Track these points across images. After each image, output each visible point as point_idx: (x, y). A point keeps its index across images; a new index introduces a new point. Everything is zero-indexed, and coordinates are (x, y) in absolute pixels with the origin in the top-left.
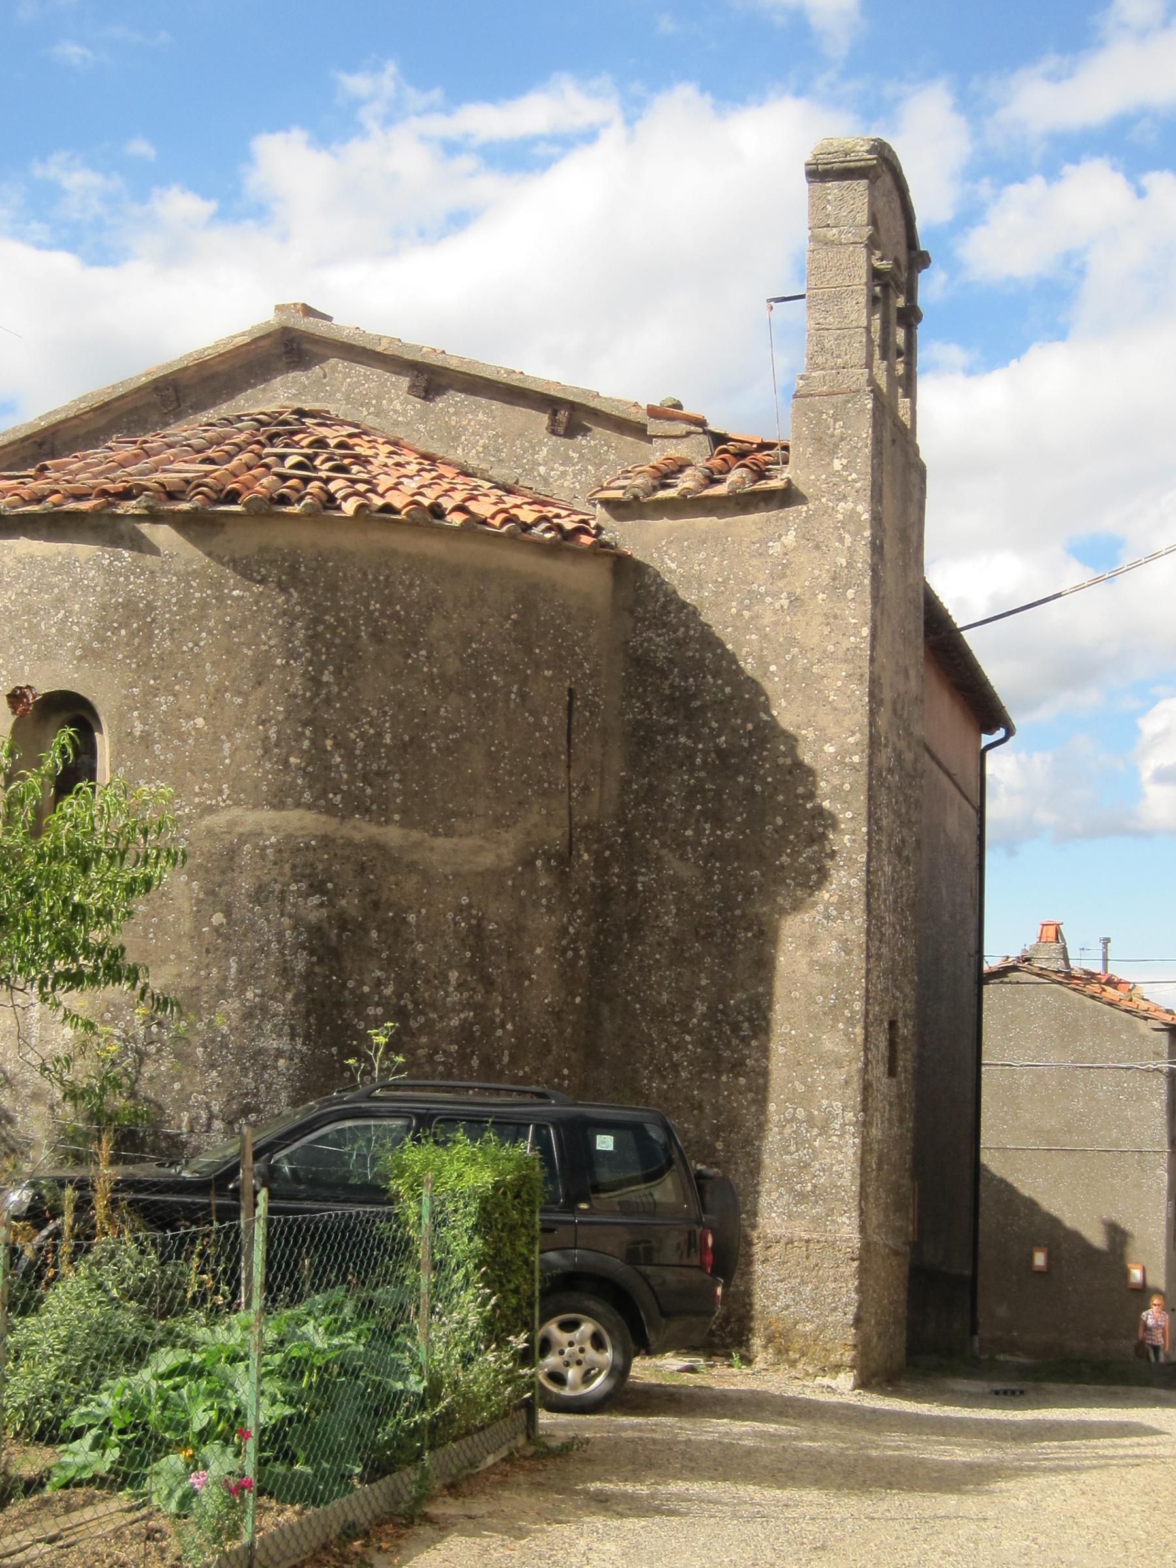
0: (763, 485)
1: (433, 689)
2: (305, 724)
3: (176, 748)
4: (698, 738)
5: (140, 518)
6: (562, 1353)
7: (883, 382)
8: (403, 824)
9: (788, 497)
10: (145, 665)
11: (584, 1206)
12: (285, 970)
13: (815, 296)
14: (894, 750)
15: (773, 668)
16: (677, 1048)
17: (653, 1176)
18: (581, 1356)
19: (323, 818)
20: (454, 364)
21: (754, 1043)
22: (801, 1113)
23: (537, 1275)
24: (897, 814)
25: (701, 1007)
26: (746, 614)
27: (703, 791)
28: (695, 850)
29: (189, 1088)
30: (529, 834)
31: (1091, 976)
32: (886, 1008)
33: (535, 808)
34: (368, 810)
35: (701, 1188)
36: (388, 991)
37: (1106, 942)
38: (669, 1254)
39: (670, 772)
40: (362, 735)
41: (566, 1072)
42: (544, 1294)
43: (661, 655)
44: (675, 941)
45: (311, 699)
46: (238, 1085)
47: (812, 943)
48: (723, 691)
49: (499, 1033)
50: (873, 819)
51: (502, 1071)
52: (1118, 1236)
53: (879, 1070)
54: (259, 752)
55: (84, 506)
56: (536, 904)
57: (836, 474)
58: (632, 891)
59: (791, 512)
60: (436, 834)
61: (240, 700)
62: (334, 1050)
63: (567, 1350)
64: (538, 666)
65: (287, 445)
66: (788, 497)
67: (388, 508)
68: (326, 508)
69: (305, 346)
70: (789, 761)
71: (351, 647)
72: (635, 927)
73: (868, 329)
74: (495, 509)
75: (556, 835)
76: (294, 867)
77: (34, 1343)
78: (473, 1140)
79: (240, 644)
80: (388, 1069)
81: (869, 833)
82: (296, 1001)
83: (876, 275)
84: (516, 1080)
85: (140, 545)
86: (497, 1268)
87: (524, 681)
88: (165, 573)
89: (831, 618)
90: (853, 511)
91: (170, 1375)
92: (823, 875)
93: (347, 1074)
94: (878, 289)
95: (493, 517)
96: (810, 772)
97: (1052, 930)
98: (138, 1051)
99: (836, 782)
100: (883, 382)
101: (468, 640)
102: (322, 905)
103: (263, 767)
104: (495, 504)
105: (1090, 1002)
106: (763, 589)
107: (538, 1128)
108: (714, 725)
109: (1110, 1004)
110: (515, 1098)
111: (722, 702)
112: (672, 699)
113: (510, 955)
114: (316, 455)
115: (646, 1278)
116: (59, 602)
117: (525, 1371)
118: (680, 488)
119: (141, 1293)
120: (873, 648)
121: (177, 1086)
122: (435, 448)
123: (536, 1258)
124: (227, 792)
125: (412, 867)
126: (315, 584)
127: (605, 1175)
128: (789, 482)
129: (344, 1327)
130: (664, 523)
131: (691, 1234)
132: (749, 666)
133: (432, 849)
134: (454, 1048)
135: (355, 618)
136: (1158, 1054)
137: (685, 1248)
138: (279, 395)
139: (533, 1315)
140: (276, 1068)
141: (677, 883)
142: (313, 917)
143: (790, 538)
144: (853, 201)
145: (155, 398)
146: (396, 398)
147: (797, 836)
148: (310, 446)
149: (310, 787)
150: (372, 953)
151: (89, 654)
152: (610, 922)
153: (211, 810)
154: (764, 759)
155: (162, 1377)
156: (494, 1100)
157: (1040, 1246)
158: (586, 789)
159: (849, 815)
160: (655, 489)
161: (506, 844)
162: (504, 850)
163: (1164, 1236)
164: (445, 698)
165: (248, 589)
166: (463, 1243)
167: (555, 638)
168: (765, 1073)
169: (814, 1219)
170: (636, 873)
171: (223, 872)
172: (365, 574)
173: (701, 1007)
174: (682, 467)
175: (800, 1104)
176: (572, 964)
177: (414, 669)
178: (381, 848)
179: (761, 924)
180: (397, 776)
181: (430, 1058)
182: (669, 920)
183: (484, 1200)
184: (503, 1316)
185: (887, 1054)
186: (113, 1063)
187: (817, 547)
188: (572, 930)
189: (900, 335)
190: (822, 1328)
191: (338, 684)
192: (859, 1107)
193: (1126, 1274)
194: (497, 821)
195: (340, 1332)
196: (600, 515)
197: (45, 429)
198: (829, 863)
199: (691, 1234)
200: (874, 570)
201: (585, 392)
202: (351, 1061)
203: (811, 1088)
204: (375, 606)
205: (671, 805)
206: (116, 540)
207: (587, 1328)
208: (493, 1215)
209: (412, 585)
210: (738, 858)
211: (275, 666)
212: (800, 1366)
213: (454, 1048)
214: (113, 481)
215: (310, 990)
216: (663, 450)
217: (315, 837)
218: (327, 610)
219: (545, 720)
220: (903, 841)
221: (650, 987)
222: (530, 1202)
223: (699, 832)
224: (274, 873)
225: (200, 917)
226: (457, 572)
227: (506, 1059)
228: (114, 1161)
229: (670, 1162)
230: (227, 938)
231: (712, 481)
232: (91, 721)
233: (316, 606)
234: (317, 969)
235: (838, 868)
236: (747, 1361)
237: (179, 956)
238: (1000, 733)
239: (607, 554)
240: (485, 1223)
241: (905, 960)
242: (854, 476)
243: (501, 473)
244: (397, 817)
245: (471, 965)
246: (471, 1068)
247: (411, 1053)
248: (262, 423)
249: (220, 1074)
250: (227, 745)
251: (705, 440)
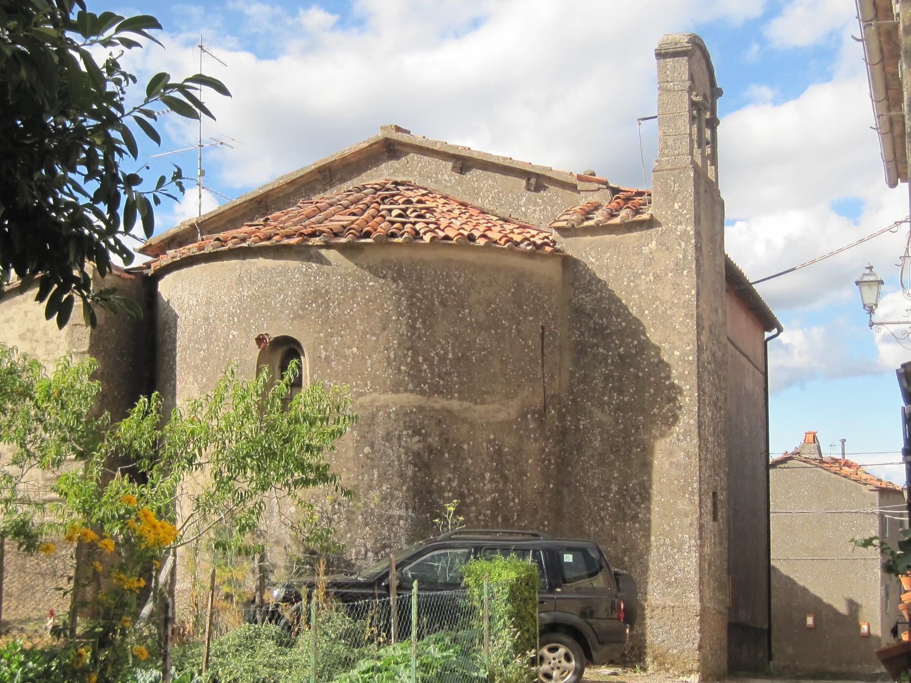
0: (638, 218)
1: (473, 329)
2: (408, 349)
3: (343, 364)
4: (609, 350)
5: (321, 247)
6: (550, 663)
7: (699, 161)
8: (459, 399)
9: (651, 223)
10: (326, 322)
11: (559, 590)
12: (402, 475)
13: (664, 118)
14: (711, 352)
15: (647, 312)
16: (603, 509)
17: (592, 575)
18: (559, 665)
19: (419, 397)
20: (475, 156)
21: (642, 506)
22: (668, 541)
23: (538, 623)
24: (714, 385)
25: (615, 488)
26: (632, 284)
27: (612, 376)
28: (609, 407)
29: (355, 536)
30: (523, 401)
31: (836, 461)
33: (527, 388)
34: (441, 392)
35: (617, 581)
36: (455, 484)
38: (602, 612)
39: (595, 367)
40: (437, 354)
41: (546, 523)
42: (542, 633)
43: (589, 307)
44: (600, 454)
45: (411, 337)
46: (380, 534)
47: (671, 453)
50: (700, 388)
51: (513, 524)
52: (854, 606)
53: (708, 518)
54: (386, 364)
55: (293, 241)
56: (529, 437)
57: (676, 211)
58: (577, 429)
59: (653, 231)
60: (476, 403)
62: (428, 515)
63: (553, 662)
64: (526, 314)
65: (391, 204)
66: (651, 223)
67: (447, 238)
68: (415, 239)
69: (397, 147)
70: (656, 360)
71: (430, 309)
72: (579, 447)
73: (690, 135)
74: (500, 235)
75: (538, 401)
76: (405, 422)
77: (297, 660)
78: (506, 558)
79: (374, 309)
80: (456, 524)
81: (699, 396)
82: (408, 490)
83: (693, 104)
84: (520, 528)
85: (321, 260)
86: (519, 618)
87: (518, 323)
88: (334, 275)
89: (676, 286)
90: (685, 230)
91: (368, 671)
92: (676, 418)
93: (435, 527)
94: (695, 112)
95: (500, 239)
96: (667, 365)
97: (811, 437)
98: (328, 518)
99: (681, 370)
100: (699, 161)
101: (489, 303)
102: (420, 441)
104: (500, 232)
105: (834, 476)
107: (535, 552)
108: (617, 342)
109: (845, 477)
110: (520, 537)
112: (595, 329)
113: (516, 464)
114: (407, 208)
115: (591, 625)
116: (281, 290)
117: (533, 668)
118: (595, 220)
119: (347, 635)
120: (698, 301)
121: (349, 535)
122: (466, 199)
123: (537, 615)
124: (369, 385)
125: (465, 421)
126: (410, 277)
127: (568, 574)
128: (652, 215)
129: (447, 648)
130: (588, 238)
131: (613, 603)
132: (634, 311)
133: (474, 411)
134: (489, 512)
135: (432, 295)
136: (873, 504)
137: (609, 610)
138: (384, 173)
139: (536, 643)
141: (600, 424)
142: (415, 448)
143: (653, 245)
144: (681, 68)
145: (319, 176)
146: (446, 171)
147: (662, 399)
148: (404, 203)
149: (412, 382)
150: (446, 465)
151: (297, 317)
152: (565, 443)
153: (361, 394)
154: (643, 360)
155: (363, 673)
156: (510, 538)
157: (810, 613)
158: (552, 377)
159: (688, 387)
160: (583, 221)
161: (512, 407)
162: (511, 410)
163: (879, 606)
164: (479, 334)
165: (377, 282)
166: (502, 608)
167: (534, 300)
168: (649, 521)
169: (676, 595)
170: (579, 420)
171: (369, 426)
172: (436, 272)
173: (615, 488)
174: (597, 207)
175: (667, 537)
176: (548, 467)
177: (463, 319)
178: (449, 411)
179: (644, 445)
181: (477, 518)
182: (597, 444)
183: (512, 586)
184: (522, 643)
186: (316, 524)
187: (667, 249)
188: (547, 450)
189: (708, 133)
190: (682, 652)
192: (697, 537)
193: (859, 628)
194: (507, 396)
195: (445, 650)
196: (555, 235)
197: (262, 195)
198: (678, 412)
199: (613, 603)
200: (697, 261)
201: (544, 168)
202: (437, 520)
203: (672, 528)
204: (442, 287)
205: (596, 384)
206: (309, 259)
207: (562, 650)
208: (518, 594)
209: (460, 276)
210: (631, 411)
211: (391, 320)
212: (671, 671)
213: (489, 512)
214: (305, 227)
215: (415, 484)
216: (586, 198)
217: (415, 407)
218: (417, 291)
219: (530, 343)
220: (717, 398)
221: (588, 478)
222: (533, 588)
223: (611, 397)
224: (395, 426)
225: (358, 450)
226: (483, 269)
227: (515, 517)
228: (326, 574)
229: (601, 567)
230: (372, 459)
231: (612, 216)
232: (299, 350)
233: (412, 289)
234: (418, 474)
235: (683, 414)
236: (644, 669)
237: (348, 469)
238: (775, 331)
239: (559, 256)
240: (513, 597)
241: (721, 460)
243: (501, 212)
245: (496, 470)
246: (497, 522)
247: (467, 515)
248: (377, 190)
249: (371, 529)
251: (608, 192)
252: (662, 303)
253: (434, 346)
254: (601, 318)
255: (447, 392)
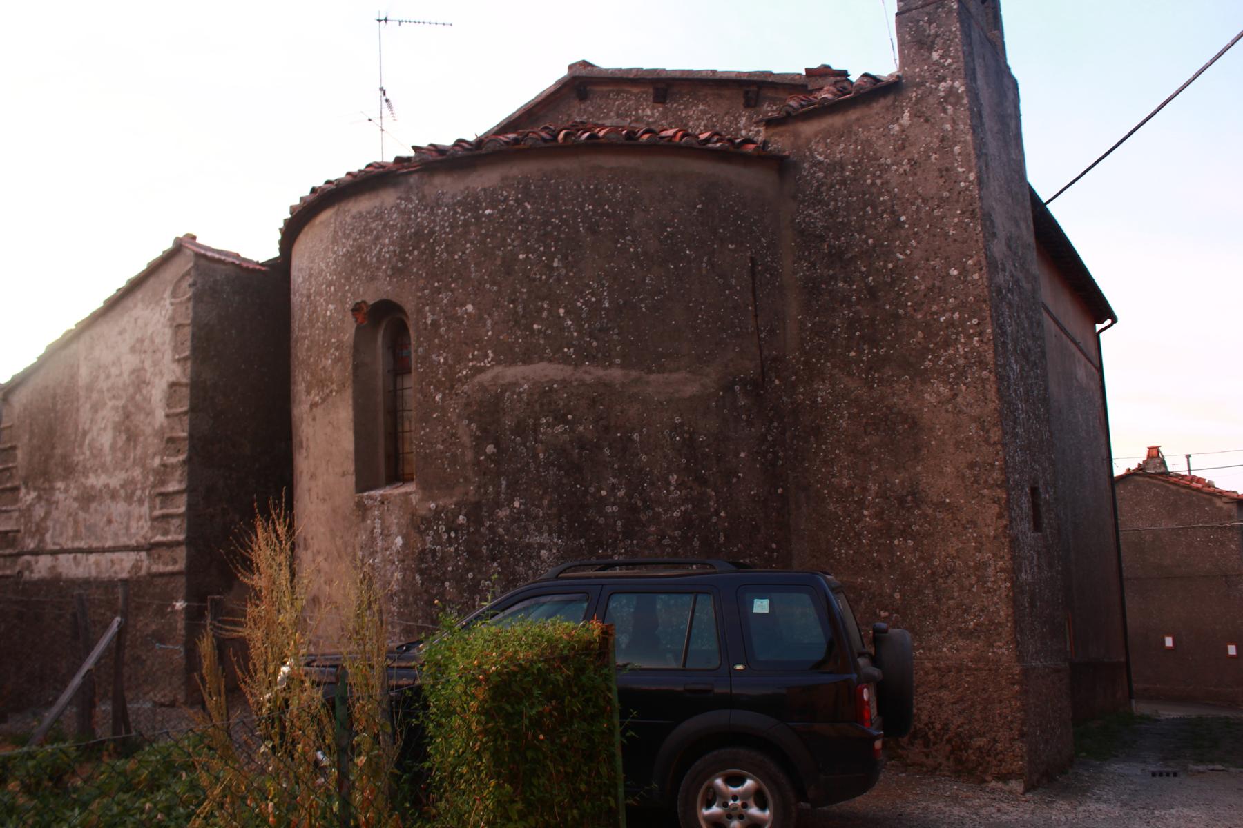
8: (622, 366)
25: (874, 488)
26: (878, 182)
28: (858, 367)
32: (1026, 477)
36: (621, 493)
37: (1188, 457)
41: (774, 546)
45: (547, 280)
48: (867, 243)
49: (714, 519)
57: (936, 63)
60: (650, 372)
61: (495, 288)
79: (493, 248)
82: (550, 506)
103: (515, 334)
106: (889, 161)
108: (864, 269)
111: (867, 251)
121: (470, 575)
133: (648, 383)
135: (575, 218)
140: (539, 557)
147: (936, 344)
151: (397, 272)
153: (481, 370)
172: (579, 186)
173: (874, 488)
180: (616, 331)
185: (1031, 513)
187: (927, 121)
188: (770, 438)
191: (566, 268)
209: (616, 190)
218: (553, 215)
225: (478, 449)
227: (722, 539)
237: (466, 479)
238: (1108, 322)
242: (950, 61)
244: (618, 361)
249: (499, 565)
250: (489, 322)
252: (925, 201)
253: (582, 292)
254: (839, 238)
255: (602, 357)
